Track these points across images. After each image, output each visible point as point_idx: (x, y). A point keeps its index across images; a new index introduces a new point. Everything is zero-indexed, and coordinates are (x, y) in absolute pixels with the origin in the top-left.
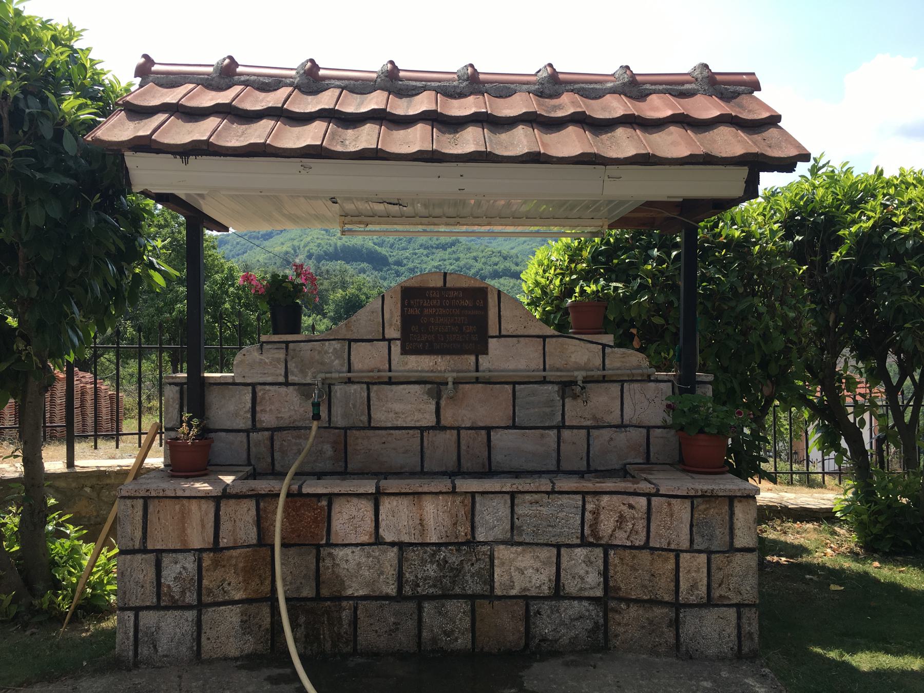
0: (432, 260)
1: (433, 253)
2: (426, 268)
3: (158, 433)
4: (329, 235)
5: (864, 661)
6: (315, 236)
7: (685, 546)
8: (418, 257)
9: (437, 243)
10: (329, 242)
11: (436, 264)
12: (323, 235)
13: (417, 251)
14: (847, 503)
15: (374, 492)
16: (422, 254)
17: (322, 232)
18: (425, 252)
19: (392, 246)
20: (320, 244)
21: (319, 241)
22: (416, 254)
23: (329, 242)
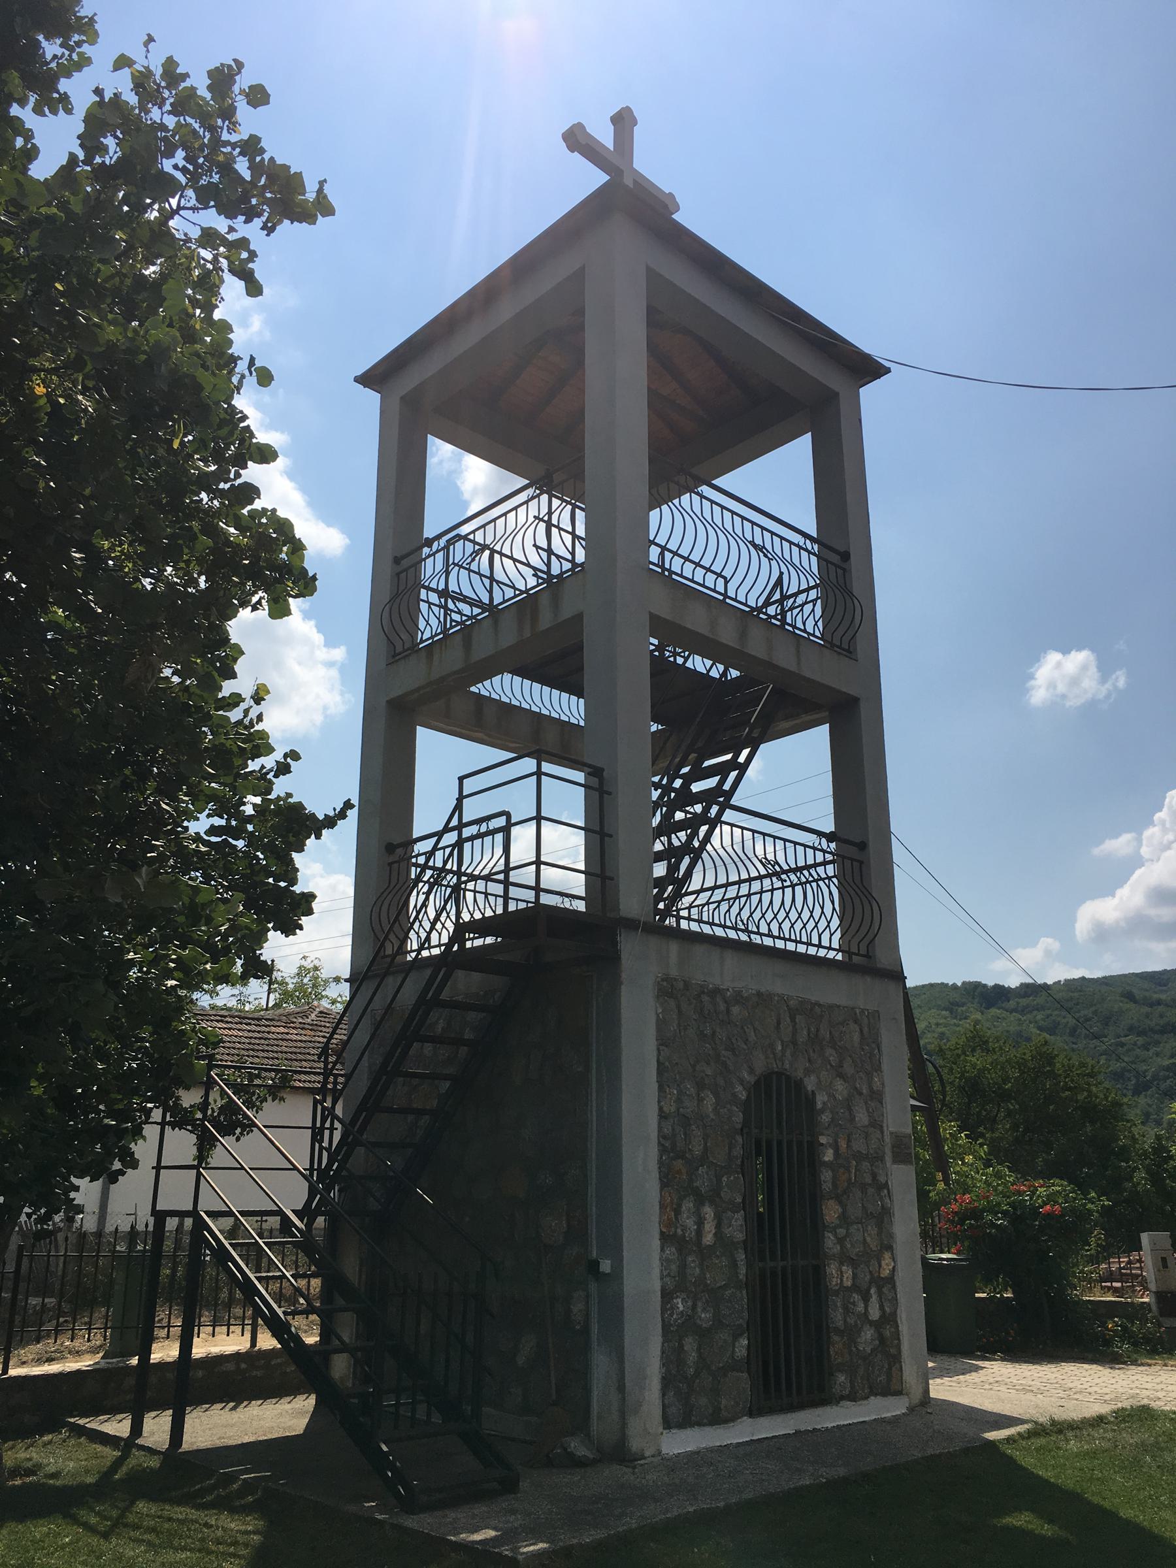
0: (1157, 1054)
1: (1157, 1043)
2: (1146, 1071)
3: (678, 913)
4: (955, 1018)
5: (214, 1244)
6: (933, 1021)
7: (156, 1438)
8: (1129, 1050)
9: (1162, 1022)
10: (958, 1029)
11: (1166, 1062)
12: (946, 1018)
13: (1123, 1039)
14: (457, 603)
15: (168, 1219)
16: (1135, 1044)
17: (944, 1012)
18: (1141, 1040)
19: (1073, 1032)
20: (943, 1034)
21: (941, 1029)
22: (1122, 1045)
23: (958, 1029)
